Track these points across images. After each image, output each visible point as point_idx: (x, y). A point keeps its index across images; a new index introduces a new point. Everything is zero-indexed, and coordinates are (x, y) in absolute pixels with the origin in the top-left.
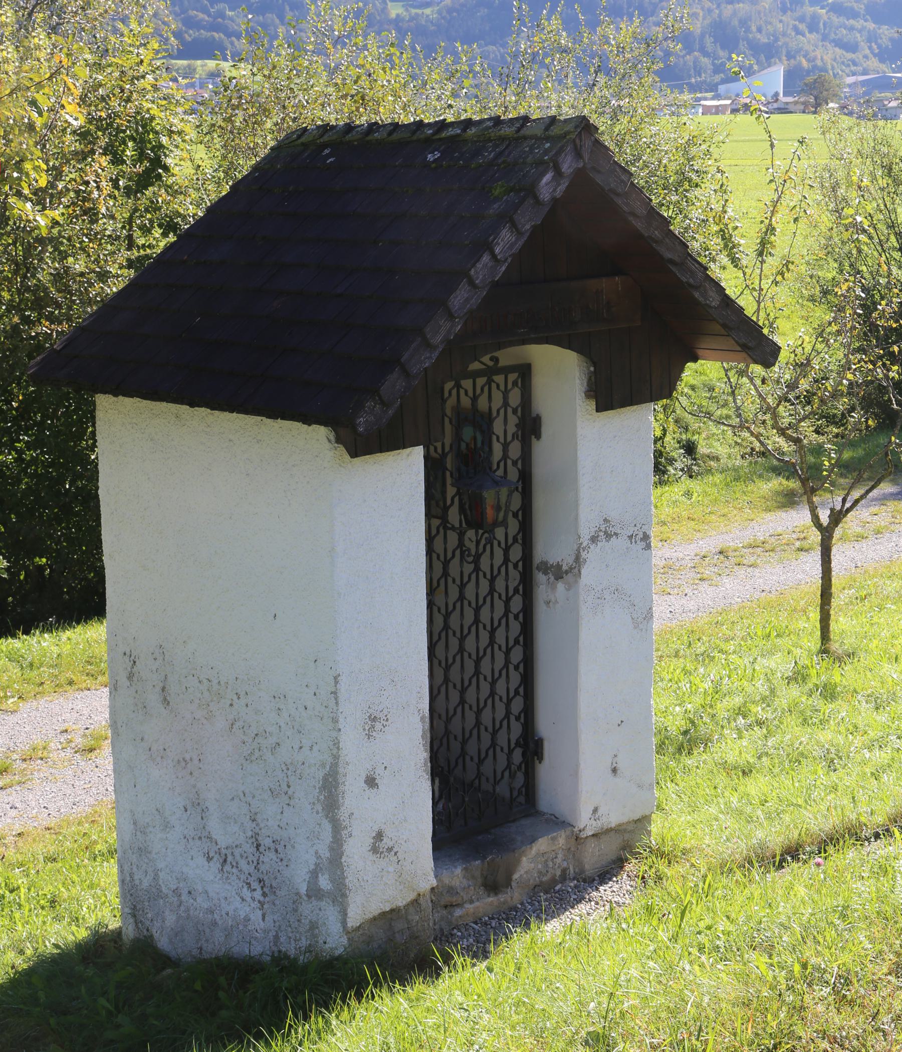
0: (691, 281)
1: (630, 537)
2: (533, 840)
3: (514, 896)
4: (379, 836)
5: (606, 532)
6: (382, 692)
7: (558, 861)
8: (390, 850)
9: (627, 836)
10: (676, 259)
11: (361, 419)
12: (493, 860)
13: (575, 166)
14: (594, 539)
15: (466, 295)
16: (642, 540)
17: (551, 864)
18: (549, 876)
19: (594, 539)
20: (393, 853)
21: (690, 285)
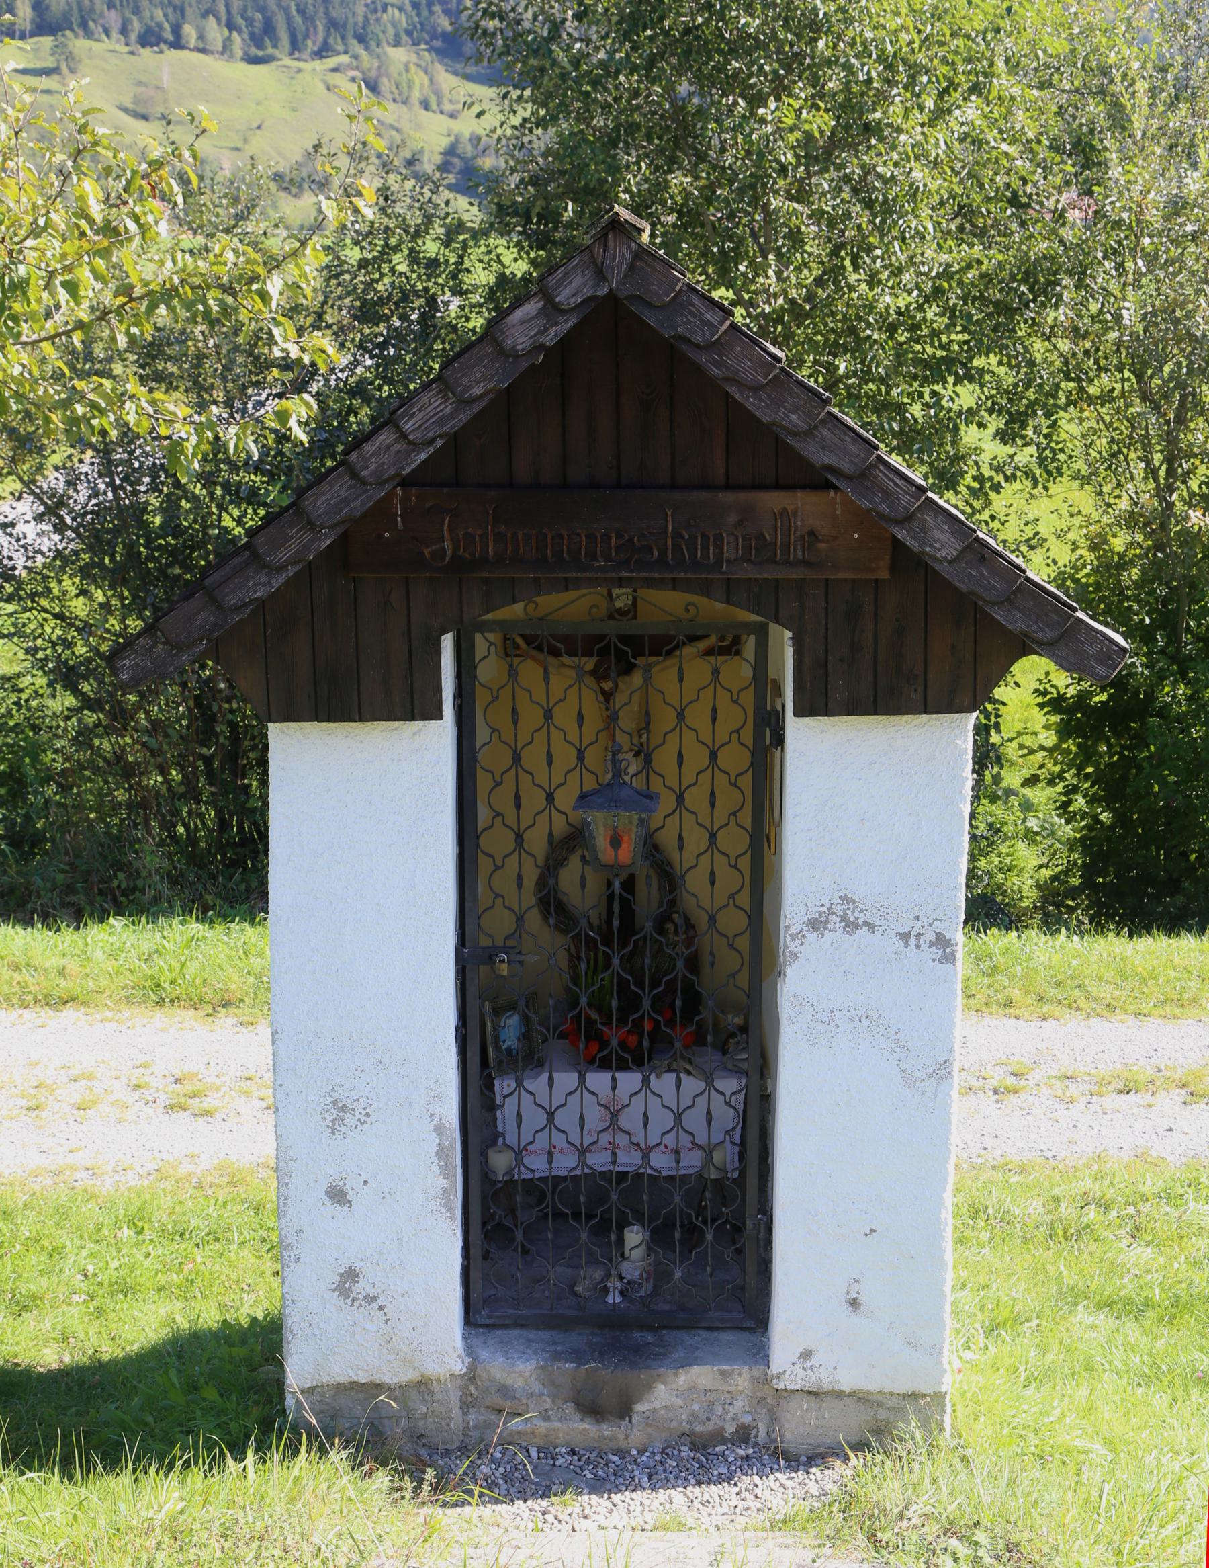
0: (883, 507)
1: (905, 936)
2: (687, 1363)
3: (631, 1434)
4: (351, 1275)
5: (844, 918)
6: (357, 1074)
7: (733, 1410)
8: (371, 1299)
9: (882, 1415)
10: (845, 466)
11: (127, 662)
12: (597, 1369)
13: (588, 292)
14: (817, 925)
15: (343, 494)
16: (931, 944)
17: (719, 1410)
18: (710, 1426)
19: (817, 925)
20: (376, 1305)
21: (881, 515)
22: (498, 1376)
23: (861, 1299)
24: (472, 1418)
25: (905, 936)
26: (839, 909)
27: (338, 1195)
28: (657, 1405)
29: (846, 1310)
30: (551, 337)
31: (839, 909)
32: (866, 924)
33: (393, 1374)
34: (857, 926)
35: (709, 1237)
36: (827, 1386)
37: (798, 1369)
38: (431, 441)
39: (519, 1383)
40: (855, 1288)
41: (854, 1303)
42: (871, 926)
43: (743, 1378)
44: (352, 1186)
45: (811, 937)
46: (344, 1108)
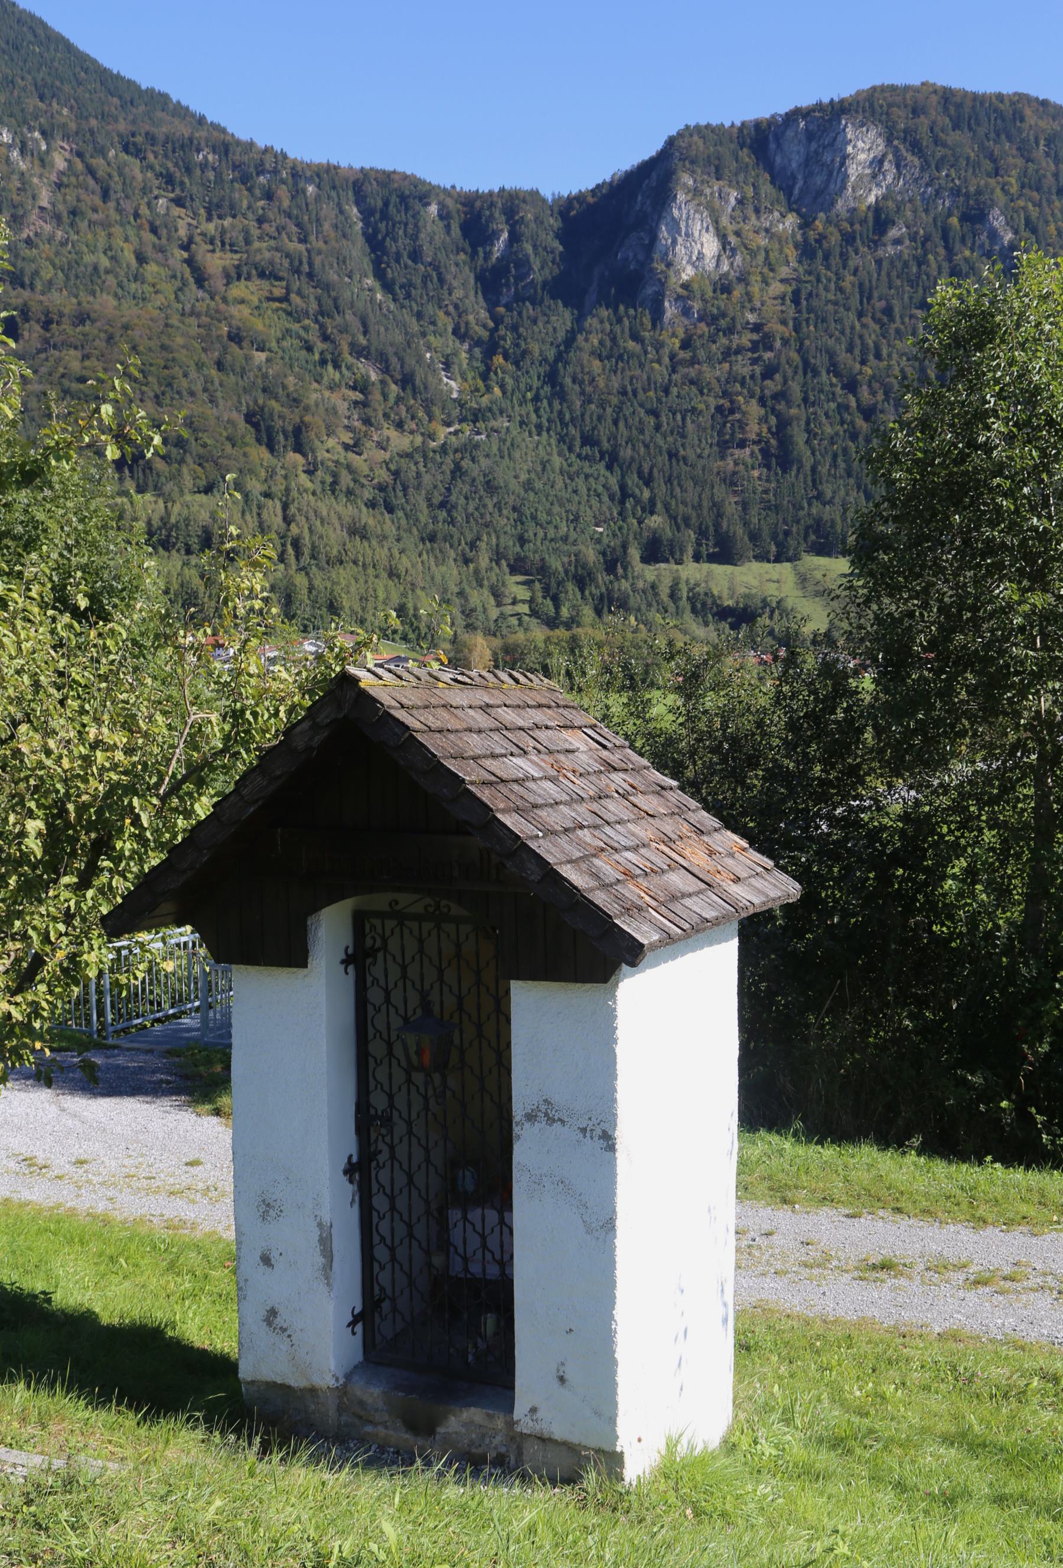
1: (584, 1130)
4: (273, 1313)
5: (546, 1114)
8: (283, 1330)
14: (531, 1117)
16: (600, 1138)
17: (487, 1441)
19: (531, 1117)
22: (359, 1393)
23: (566, 1377)
24: (343, 1418)
25: (584, 1130)
26: (543, 1108)
27: (266, 1260)
28: (450, 1430)
29: (556, 1383)
30: (317, 741)
31: (543, 1108)
32: (560, 1120)
33: (296, 1381)
34: (554, 1121)
35: (465, 1316)
36: (546, 1435)
37: (528, 1419)
38: (257, 801)
39: (370, 1401)
40: (562, 1369)
41: (562, 1379)
42: (563, 1122)
43: (500, 1423)
44: (274, 1255)
45: (527, 1125)
46: (268, 1205)
